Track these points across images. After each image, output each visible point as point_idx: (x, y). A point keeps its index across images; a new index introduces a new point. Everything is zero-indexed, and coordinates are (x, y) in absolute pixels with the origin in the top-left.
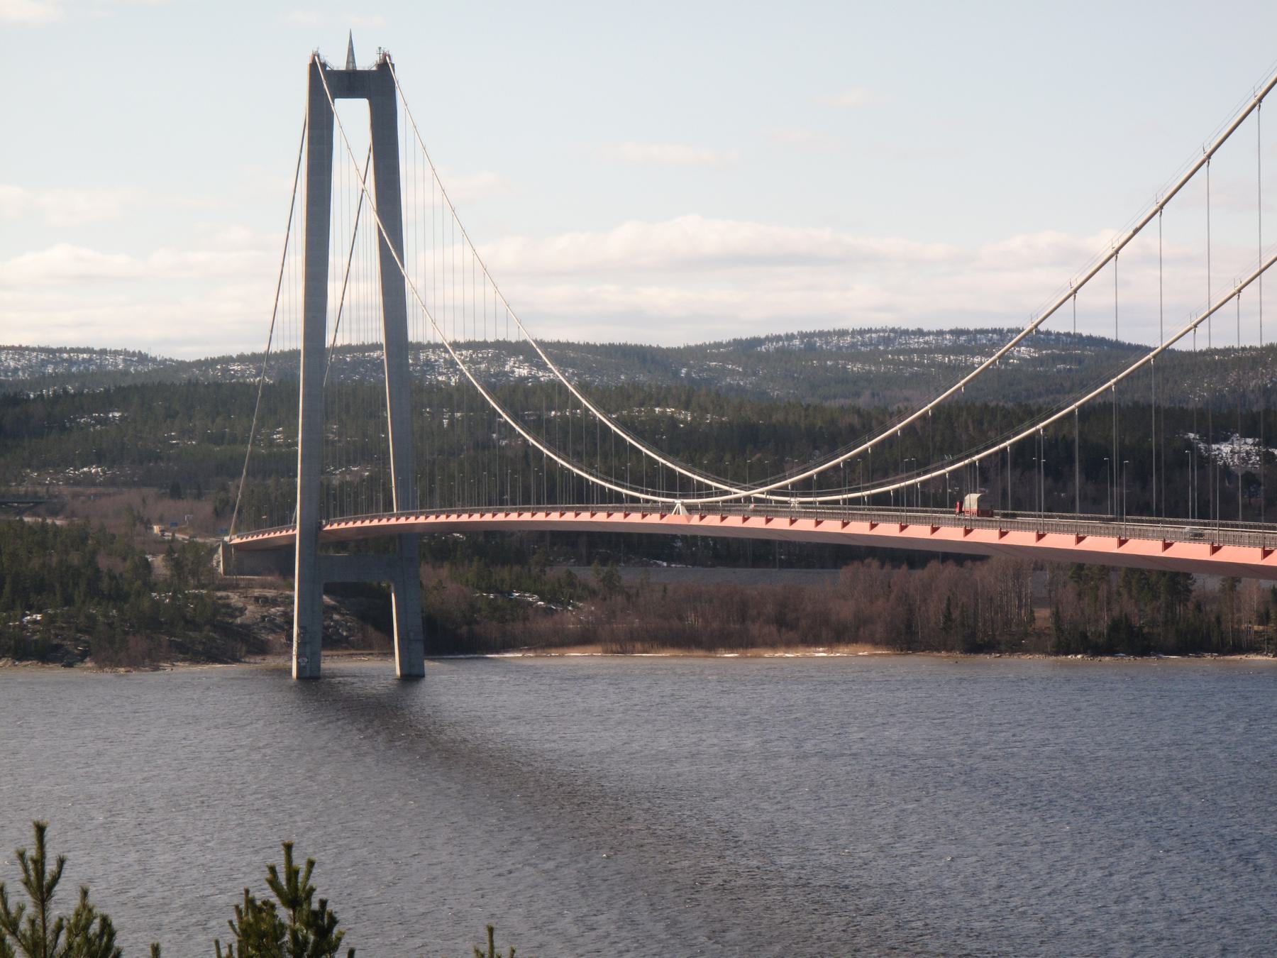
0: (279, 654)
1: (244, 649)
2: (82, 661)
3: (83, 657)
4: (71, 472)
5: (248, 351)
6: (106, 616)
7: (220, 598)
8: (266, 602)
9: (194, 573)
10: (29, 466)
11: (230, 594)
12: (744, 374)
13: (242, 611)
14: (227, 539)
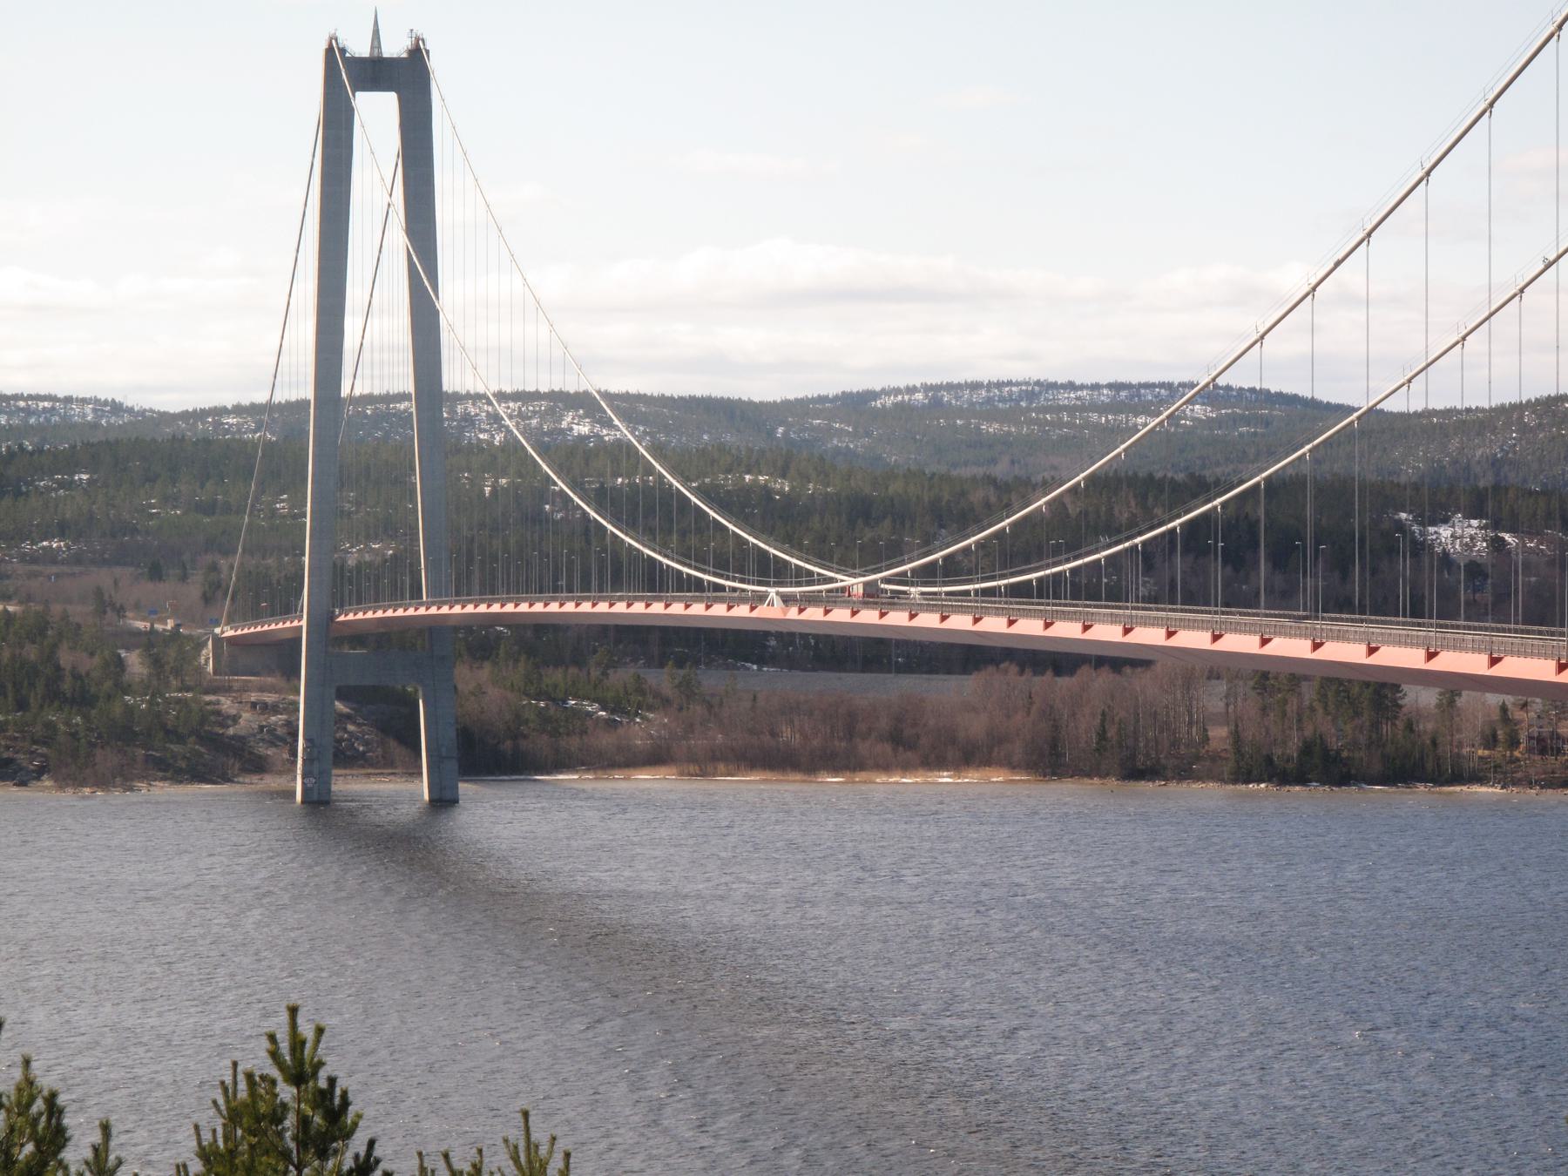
0: (280, 773)
1: (237, 766)
2: (38, 778)
3: (40, 773)
4: (27, 546)
5: (246, 402)
7: (209, 703)
8: (266, 708)
9: (177, 672)
11: (222, 699)
12: (855, 435)
13: (235, 719)
14: (218, 630)
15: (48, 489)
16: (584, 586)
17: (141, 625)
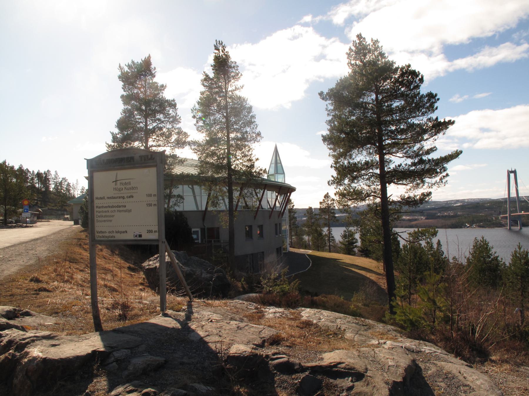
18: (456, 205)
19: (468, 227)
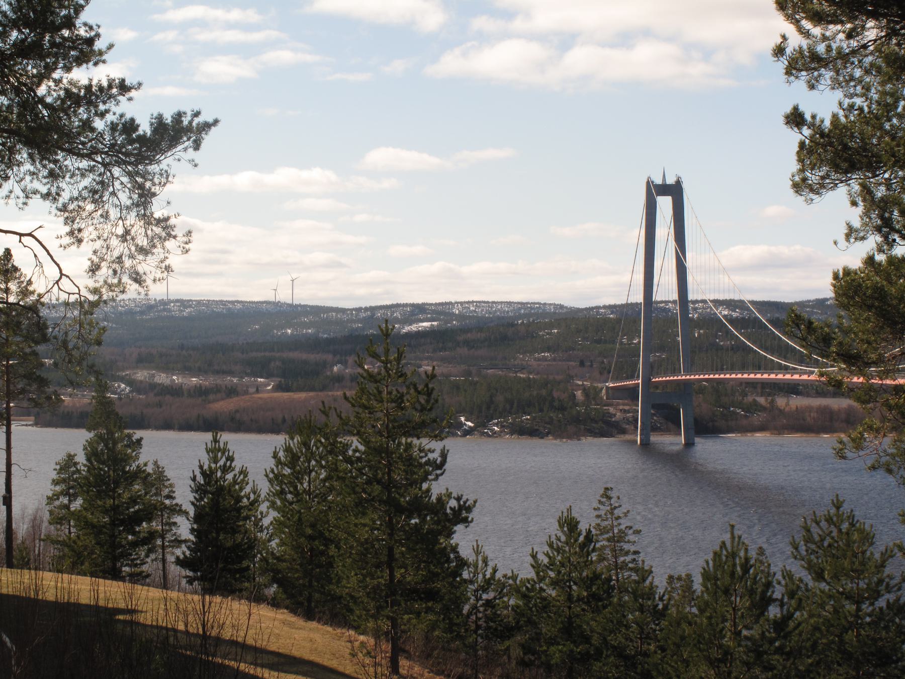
0: (631, 434)
3: (547, 434)
4: (536, 355)
5: (607, 304)
6: (557, 417)
8: (625, 411)
9: (594, 399)
10: (519, 353)
14: (607, 384)
15: (543, 335)
16: (743, 368)
17: (580, 383)
18: (414, 328)
19: (469, 432)
